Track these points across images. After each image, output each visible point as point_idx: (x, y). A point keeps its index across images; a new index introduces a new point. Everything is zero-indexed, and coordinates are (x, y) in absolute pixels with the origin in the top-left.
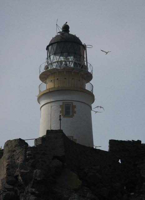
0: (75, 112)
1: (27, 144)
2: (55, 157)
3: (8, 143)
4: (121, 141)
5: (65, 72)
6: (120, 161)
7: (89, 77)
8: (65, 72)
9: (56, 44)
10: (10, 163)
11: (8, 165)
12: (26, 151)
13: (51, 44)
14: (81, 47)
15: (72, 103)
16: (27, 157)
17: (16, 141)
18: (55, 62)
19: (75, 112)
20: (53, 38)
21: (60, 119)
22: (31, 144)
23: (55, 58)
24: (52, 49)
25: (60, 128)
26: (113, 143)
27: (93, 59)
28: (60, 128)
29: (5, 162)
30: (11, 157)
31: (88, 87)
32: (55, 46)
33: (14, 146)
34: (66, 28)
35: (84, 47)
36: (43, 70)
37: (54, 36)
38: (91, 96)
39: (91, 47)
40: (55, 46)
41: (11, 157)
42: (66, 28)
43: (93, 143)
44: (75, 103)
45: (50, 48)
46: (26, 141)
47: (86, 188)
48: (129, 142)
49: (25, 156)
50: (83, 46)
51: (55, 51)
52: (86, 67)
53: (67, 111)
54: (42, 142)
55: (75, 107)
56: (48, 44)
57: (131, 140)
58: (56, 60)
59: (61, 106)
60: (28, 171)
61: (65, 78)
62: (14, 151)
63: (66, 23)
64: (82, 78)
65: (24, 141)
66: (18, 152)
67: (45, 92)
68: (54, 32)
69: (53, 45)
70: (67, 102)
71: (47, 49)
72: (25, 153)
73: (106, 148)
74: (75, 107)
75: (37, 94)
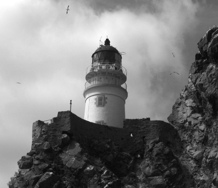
2: (64, 132)
4: (76, 115)
6: (132, 135)
9: (101, 52)
12: (42, 129)
13: (96, 52)
16: (42, 133)
23: (97, 64)
24: (97, 56)
28: (71, 110)
30: (34, 136)
32: (100, 54)
34: (107, 42)
36: (89, 72)
39: (125, 54)
40: (100, 54)
42: (107, 42)
43: (90, 122)
45: (95, 55)
48: (78, 117)
49: (41, 133)
51: (99, 57)
57: (135, 119)
60: (41, 143)
65: (43, 122)
66: (37, 130)
67: (92, 87)
71: (93, 56)
72: (41, 131)
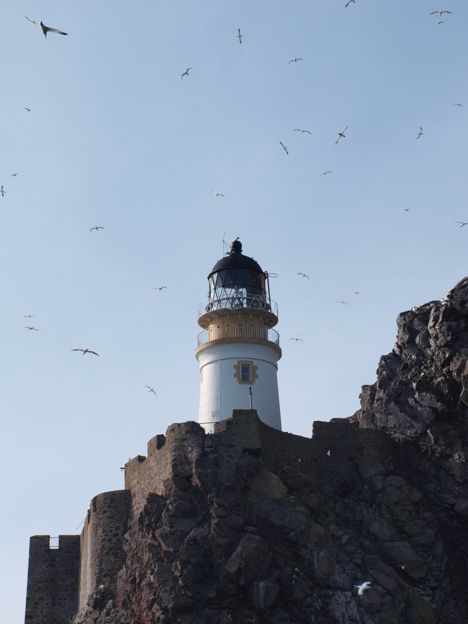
0: (257, 376)
1: (203, 430)
3: (174, 428)
5: (240, 314)
6: (329, 453)
7: (272, 320)
8: (240, 314)
9: (226, 271)
10: (178, 457)
11: (174, 460)
14: (262, 276)
15: (252, 362)
17: (187, 424)
18: (224, 299)
19: (257, 376)
20: (219, 262)
21: (251, 392)
22: (209, 429)
25: (252, 407)
26: (318, 426)
27: (278, 294)
29: (168, 456)
31: (271, 336)
32: (224, 273)
33: (183, 432)
34: (237, 246)
35: (265, 276)
36: (204, 312)
37: (221, 258)
38: (275, 350)
41: (180, 449)
42: (237, 246)
44: (256, 363)
46: (202, 426)
47: (293, 497)
49: (203, 448)
50: (264, 274)
52: (269, 307)
53: (245, 373)
54: (227, 429)
55: (256, 368)
56: (211, 272)
58: (225, 297)
59: (235, 367)
61: (251, 325)
62: (185, 440)
63: (238, 238)
64: (265, 323)
65: (199, 424)
68: (223, 251)
69: (220, 272)
70: (244, 361)
73: (307, 433)
74: (256, 368)
75: (195, 349)
